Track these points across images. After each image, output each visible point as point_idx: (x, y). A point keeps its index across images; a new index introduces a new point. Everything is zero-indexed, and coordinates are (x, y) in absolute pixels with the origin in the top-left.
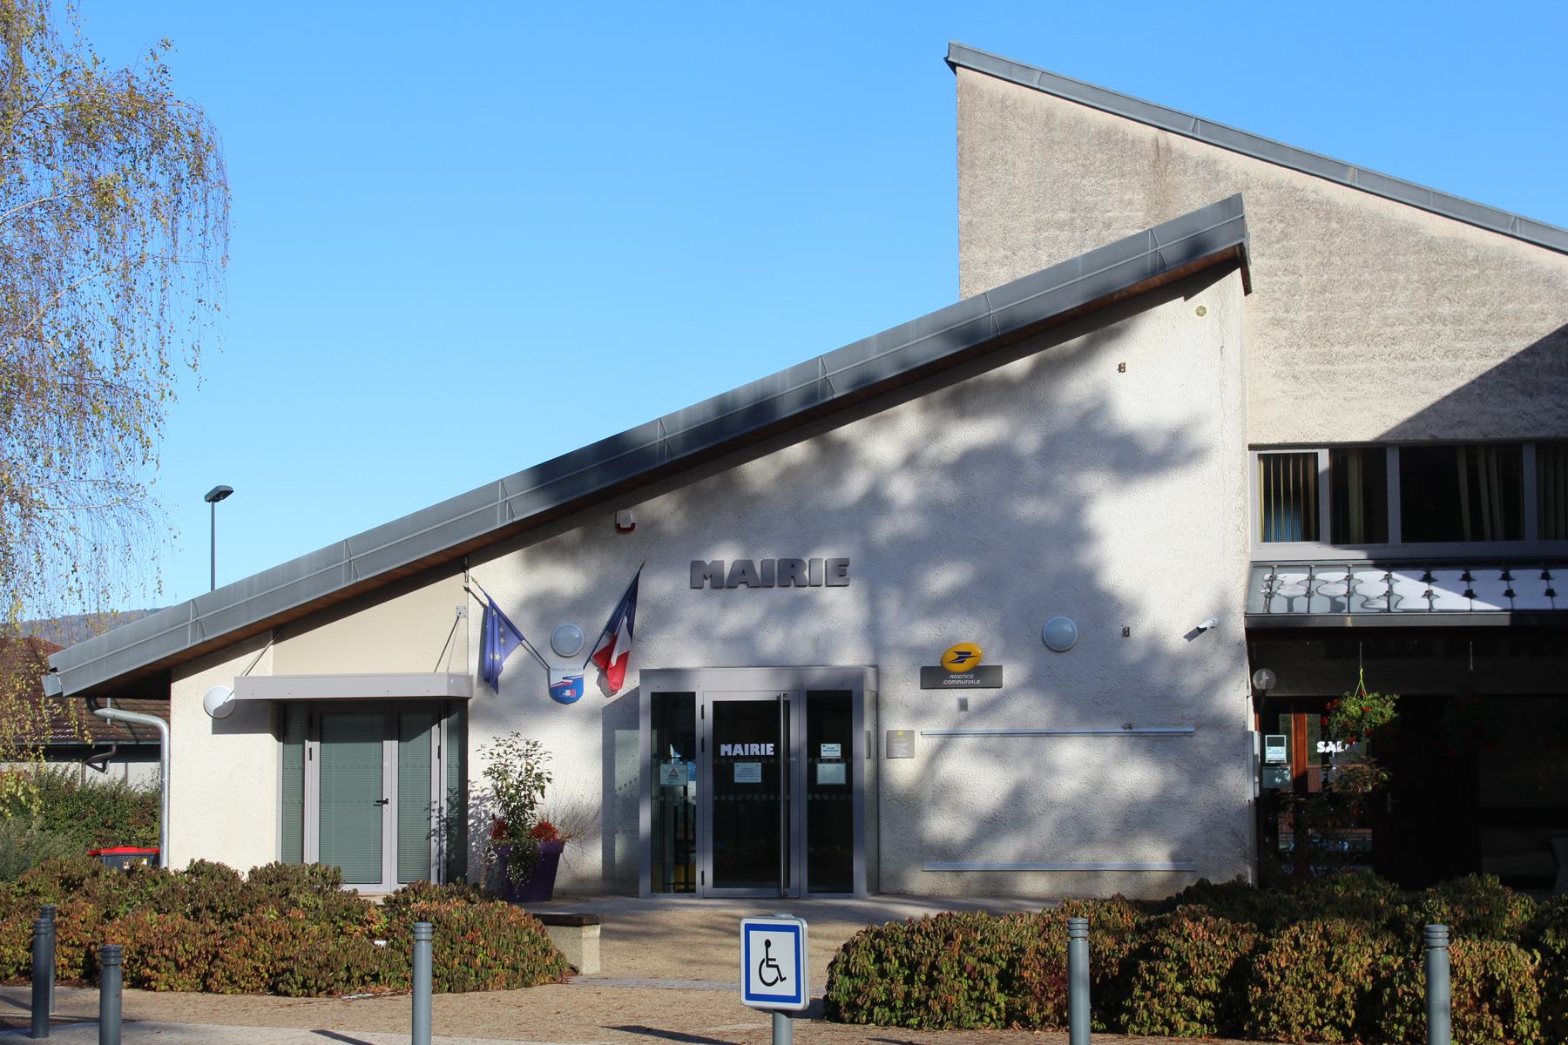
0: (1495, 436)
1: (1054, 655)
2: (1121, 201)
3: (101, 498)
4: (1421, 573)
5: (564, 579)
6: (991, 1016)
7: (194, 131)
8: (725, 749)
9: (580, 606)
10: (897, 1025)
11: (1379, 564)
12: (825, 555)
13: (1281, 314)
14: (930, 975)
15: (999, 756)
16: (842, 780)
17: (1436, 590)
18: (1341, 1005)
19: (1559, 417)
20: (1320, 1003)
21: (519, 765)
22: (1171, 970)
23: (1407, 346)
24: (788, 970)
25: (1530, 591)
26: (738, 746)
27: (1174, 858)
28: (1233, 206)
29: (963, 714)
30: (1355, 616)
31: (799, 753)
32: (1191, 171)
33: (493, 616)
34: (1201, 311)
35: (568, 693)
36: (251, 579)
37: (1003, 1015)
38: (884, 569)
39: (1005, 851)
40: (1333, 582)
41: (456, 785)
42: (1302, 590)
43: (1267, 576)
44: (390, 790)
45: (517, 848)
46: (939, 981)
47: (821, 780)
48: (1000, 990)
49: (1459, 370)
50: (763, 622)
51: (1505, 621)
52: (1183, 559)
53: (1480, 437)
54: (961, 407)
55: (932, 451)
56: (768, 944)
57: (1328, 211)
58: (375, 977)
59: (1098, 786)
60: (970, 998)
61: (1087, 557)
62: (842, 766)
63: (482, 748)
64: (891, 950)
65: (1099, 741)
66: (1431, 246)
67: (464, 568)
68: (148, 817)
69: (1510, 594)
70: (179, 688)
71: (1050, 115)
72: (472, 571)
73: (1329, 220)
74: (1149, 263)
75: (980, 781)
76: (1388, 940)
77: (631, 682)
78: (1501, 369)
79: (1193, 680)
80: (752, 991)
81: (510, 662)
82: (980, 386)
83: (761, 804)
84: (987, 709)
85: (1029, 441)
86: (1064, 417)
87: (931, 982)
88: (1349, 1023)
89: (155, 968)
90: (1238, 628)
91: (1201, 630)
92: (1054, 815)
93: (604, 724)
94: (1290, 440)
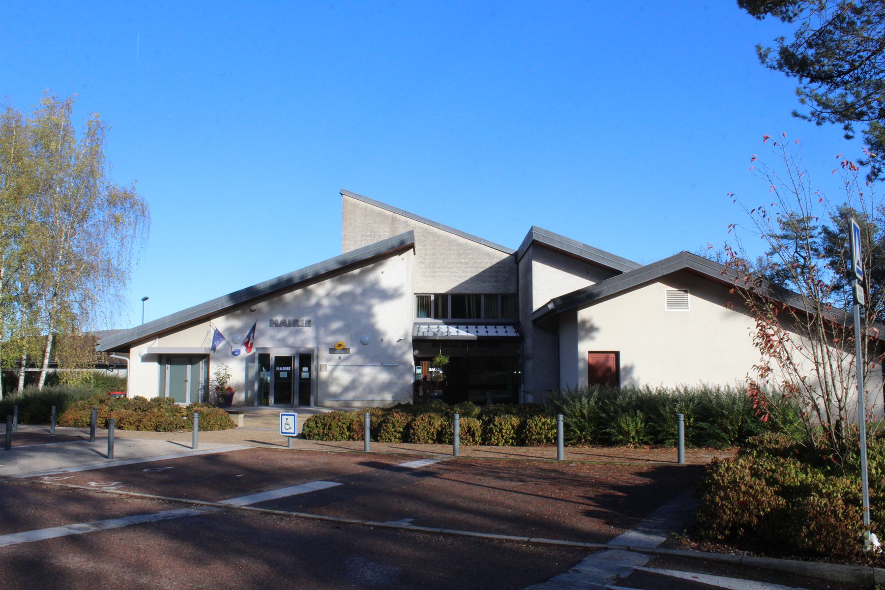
3: (113, 299)
5: (236, 323)
8: (278, 368)
9: (240, 330)
11: (446, 324)
12: (305, 319)
15: (349, 371)
21: (223, 372)
23: (453, 270)
24: (292, 426)
25: (482, 331)
28: (411, 233)
38: (320, 323)
39: (350, 395)
40: (434, 328)
44: (189, 378)
52: (397, 322)
54: (341, 281)
55: (334, 292)
57: (435, 235)
59: (374, 379)
63: (214, 367)
66: (460, 245)
70: (132, 350)
71: (366, 208)
72: (212, 321)
75: (344, 377)
78: (477, 276)
79: (399, 352)
81: (220, 345)
82: (346, 276)
85: (359, 290)
87: (330, 429)
90: (410, 339)
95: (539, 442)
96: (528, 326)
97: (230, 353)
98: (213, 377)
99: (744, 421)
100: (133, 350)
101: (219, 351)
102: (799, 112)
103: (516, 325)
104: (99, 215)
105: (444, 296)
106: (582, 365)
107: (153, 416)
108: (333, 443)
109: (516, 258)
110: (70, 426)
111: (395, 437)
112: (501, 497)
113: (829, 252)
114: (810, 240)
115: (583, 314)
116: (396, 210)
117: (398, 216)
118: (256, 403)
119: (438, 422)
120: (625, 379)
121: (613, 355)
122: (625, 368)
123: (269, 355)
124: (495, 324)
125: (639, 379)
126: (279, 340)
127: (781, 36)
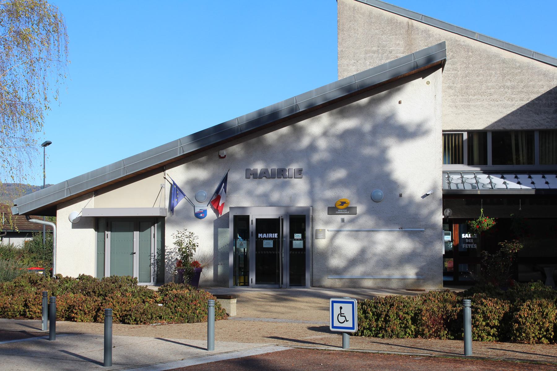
0: (525, 128)
1: (375, 203)
2: (395, 44)
4: (501, 176)
5: (200, 173)
6: (409, 334)
7: (55, 14)
8: (260, 235)
9: (206, 183)
10: (373, 336)
11: (485, 172)
12: (294, 167)
13: (451, 85)
14: (385, 319)
15: (356, 238)
16: (302, 247)
17: (507, 182)
18: (547, 330)
19: (548, 122)
20: (540, 330)
21: (186, 241)
22: (480, 317)
23: (495, 96)
24: (349, 318)
25: (540, 183)
26: (265, 235)
27: (417, 274)
28: (442, 45)
29: (343, 223)
30: (481, 190)
31: (287, 236)
32: (420, 34)
33: (174, 187)
34: (428, 83)
35: (201, 215)
36: (88, 173)
37: (414, 333)
38: (315, 172)
41: (160, 247)
42: (460, 181)
43: (447, 176)
44: (136, 249)
45: (186, 270)
46: (389, 321)
47: (294, 247)
48: (412, 324)
49: (513, 105)
50: (272, 191)
51: (533, 192)
52: (420, 170)
53: (520, 129)
54: (343, 115)
56: (341, 308)
57: (468, 49)
58: (161, 318)
59: (391, 248)
60: (401, 327)
61: (388, 168)
62: (302, 242)
63: (171, 236)
64: (369, 309)
65: (391, 233)
66: (504, 61)
67: (164, 170)
68: (22, 257)
69: (533, 183)
72: (167, 172)
73: (468, 52)
74: (412, 65)
75: (349, 246)
78: (528, 105)
79: (425, 212)
80: (352, 326)
82: (350, 107)
83: (273, 256)
84: (352, 221)
85: (367, 127)
86: (379, 119)
87: (386, 321)
88: (552, 337)
89: (76, 313)
90: (440, 194)
91: (427, 195)
92: (375, 259)
93: (214, 226)
94: (454, 129)
98: (170, 244)
100: (61, 213)
101: (179, 212)
111: (489, 334)
118: (231, 282)
123: (248, 217)
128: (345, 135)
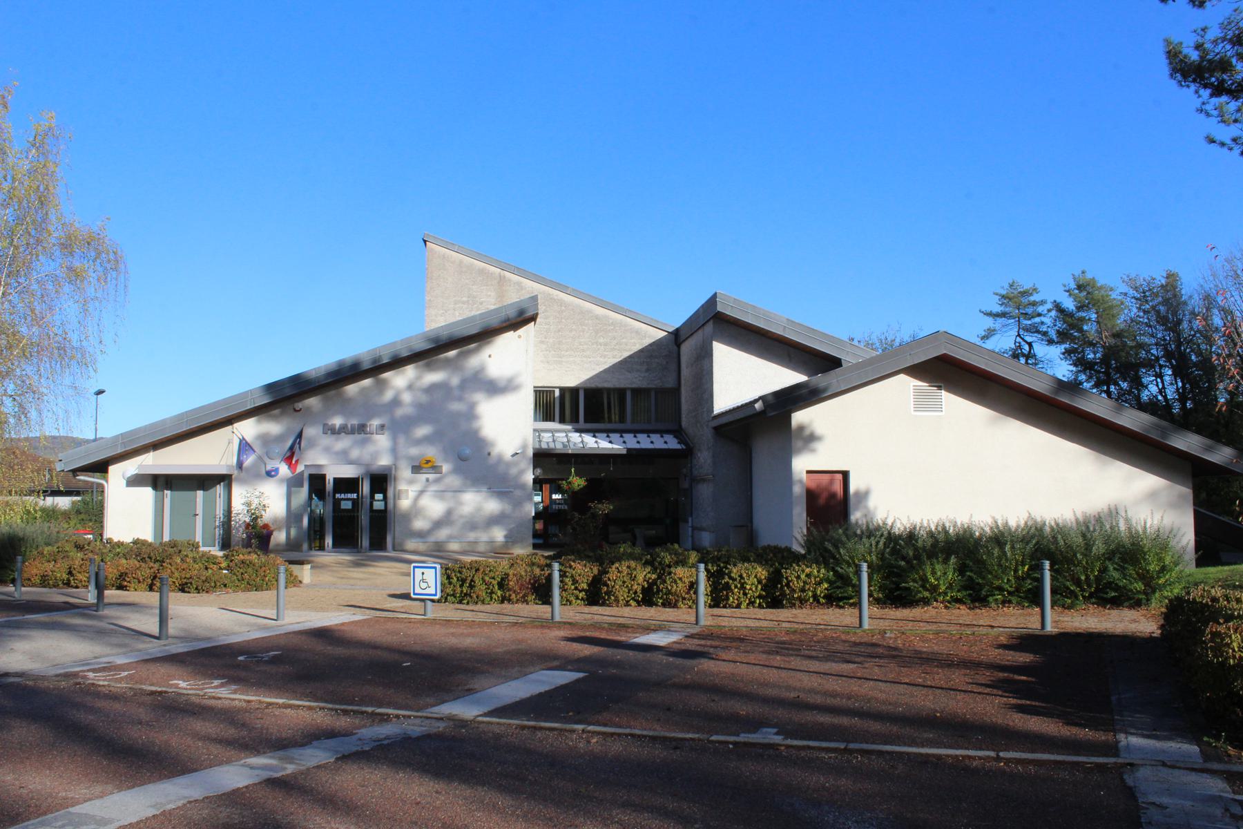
3: (70, 392)
5: (273, 427)
8: (338, 496)
9: (280, 439)
11: (577, 431)
18: (636, 593)
25: (632, 442)
27: (506, 537)
28: (534, 299)
38: (399, 428)
39: (443, 534)
40: (561, 437)
44: (199, 510)
51: (625, 452)
52: (510, 428)
54: (430, 367)
57: (561, 303)
59: (479, 509)
61: (475, 425)
66: (597, 317)
70: (112, 469)
71: (461, 262)
75: (434, 507)
76: (649, 569)
77: (300, 468)
78: (621, 363)
79: (514, 471)
81: (249, 461)
85: (455, 381)
87: (471, 587)
90: (530, 453)
95: (802, 601)
96: (703, 436)
97: (264, 472)
98: (238, 504)
99: (1104, 570)
101: (248, 470)
102: (1218, 138)
103: (678, 433)
104: (46, 266)
105: (574, 391)
106: (797, 490)
107: (157, 566)
108: (479, 607)
109: (677, 337)
110: (34, 585)
111: (577, 598)
112: (854, 687)
113: (1063, 336)
114: (1037, 320)
115: (799, 417)
116: (504, 267)
117: (507, 274)
118: (305, 546)
119: (643, 575)
120: (857, 509)
121: (840, 477)
122: (857, 493)
124: (648, 432)
125: (876, 508)
126: (337, 453)
127: (1203, 26)
128: (432, 389)
